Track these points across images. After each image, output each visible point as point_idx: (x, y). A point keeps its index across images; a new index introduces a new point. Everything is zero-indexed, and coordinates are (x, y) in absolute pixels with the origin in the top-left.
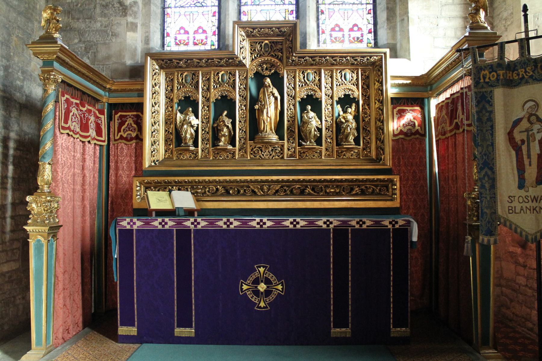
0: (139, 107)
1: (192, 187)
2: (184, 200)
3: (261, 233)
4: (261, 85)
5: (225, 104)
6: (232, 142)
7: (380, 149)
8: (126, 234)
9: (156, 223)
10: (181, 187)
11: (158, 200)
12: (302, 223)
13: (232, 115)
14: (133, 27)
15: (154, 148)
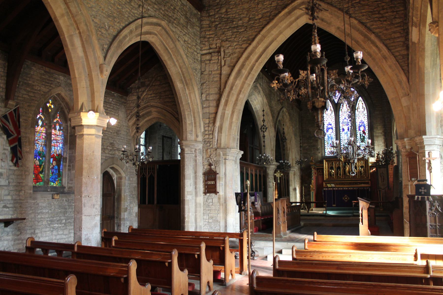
0: (323, 169)
1: (334, 183)
2: (333, 185)
3: (346, 190)
4: (345, 164)
5: (339, 168)
6: (340, 175)
7: (368, 176)
8: (325, 190)
9: (329, 189)
10: (332, 183)
11: (329, 185)
12: (352, 188)
13: (340, 170)
14: (319, 153)
15: (326, 176)
